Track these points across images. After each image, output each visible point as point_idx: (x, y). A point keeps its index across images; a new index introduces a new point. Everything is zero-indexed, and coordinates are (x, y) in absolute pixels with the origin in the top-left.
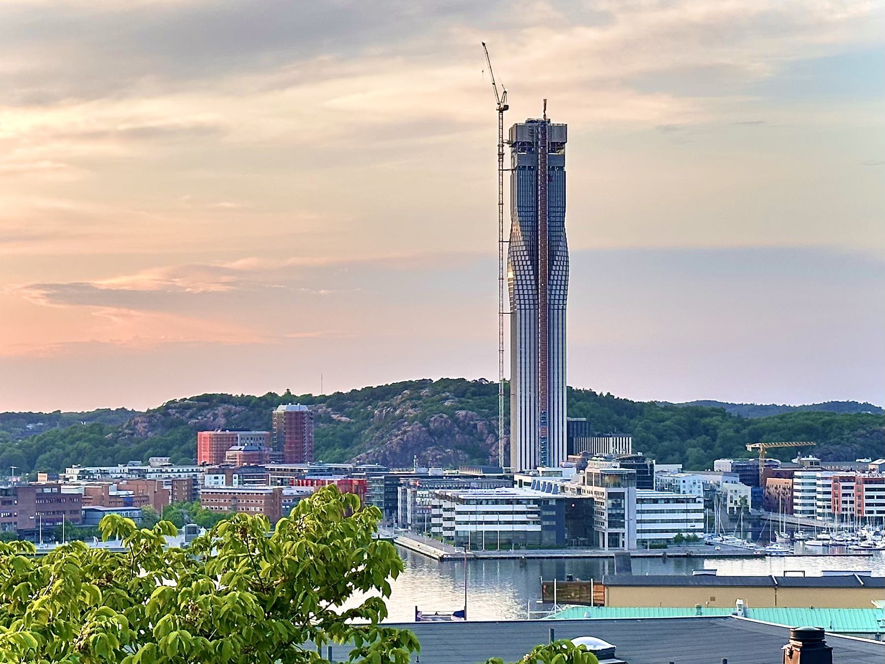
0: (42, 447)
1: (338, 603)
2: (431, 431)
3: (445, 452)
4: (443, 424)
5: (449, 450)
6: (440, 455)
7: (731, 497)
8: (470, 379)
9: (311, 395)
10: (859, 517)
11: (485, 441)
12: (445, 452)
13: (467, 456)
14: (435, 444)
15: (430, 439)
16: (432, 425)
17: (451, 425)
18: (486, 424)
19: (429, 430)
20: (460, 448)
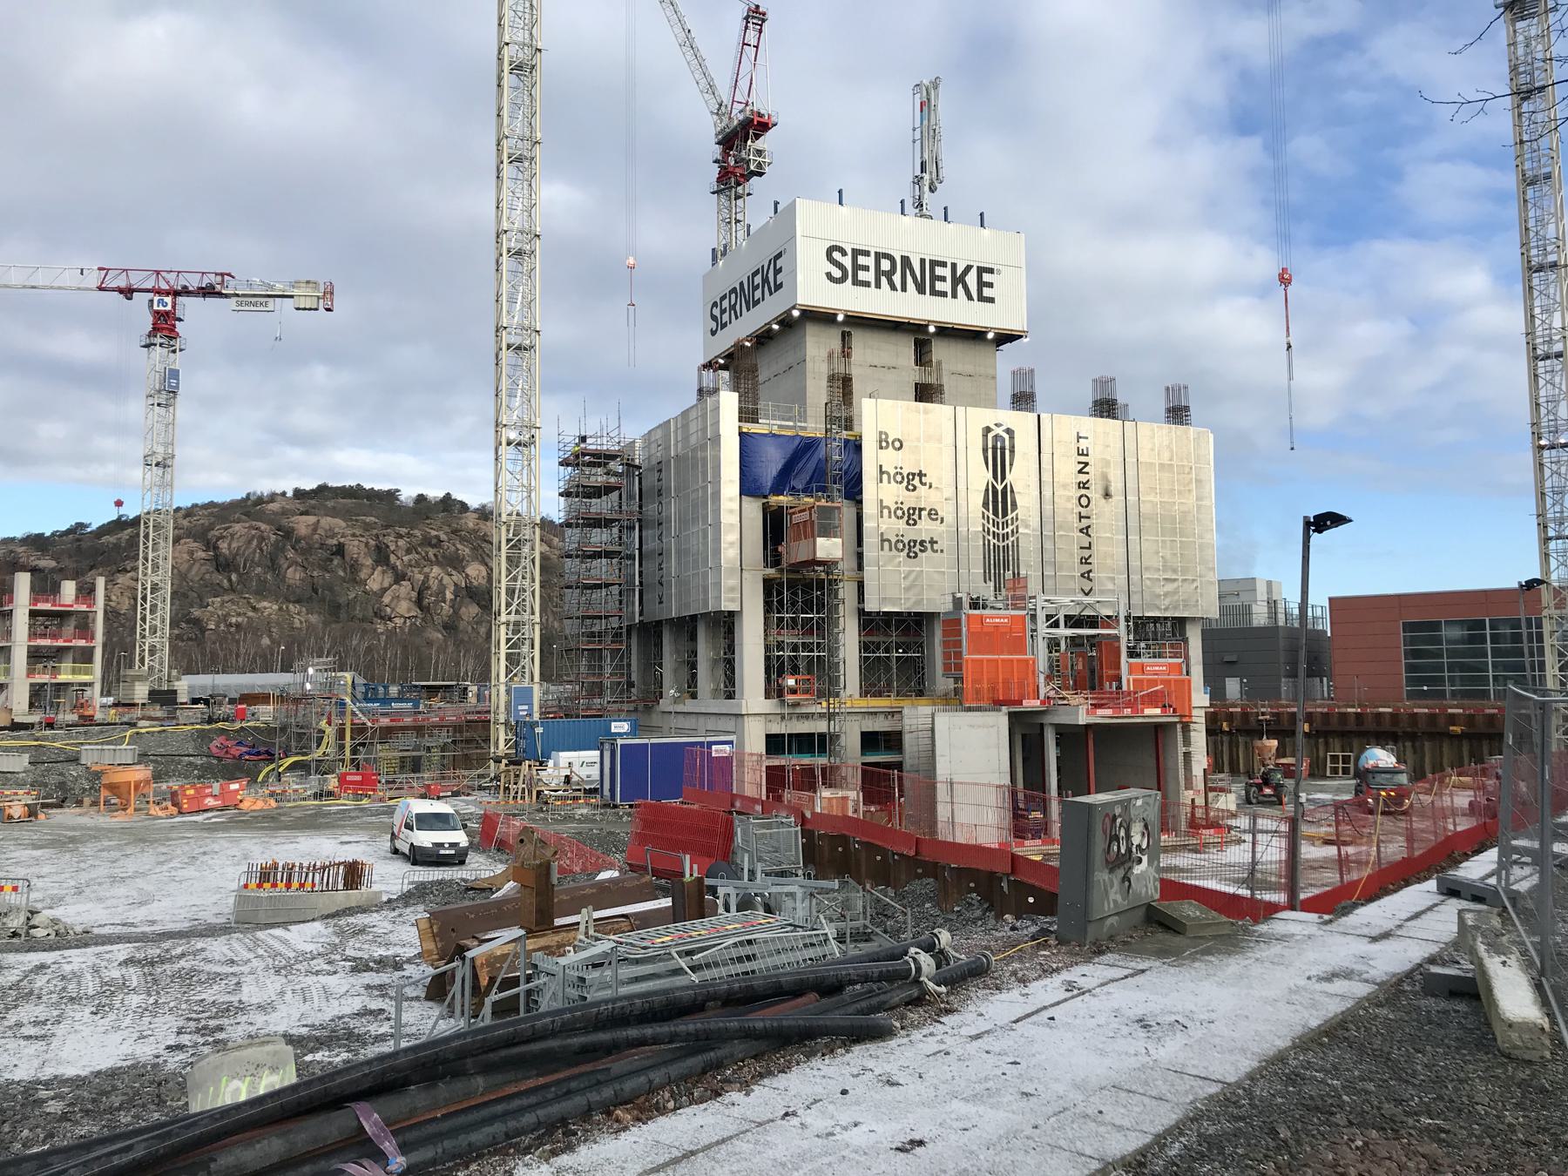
0: (783, 718)
1: (495, 1004)
2: (221, 559)
3: (254, 609)
4: (255, 542)
5: (265, 604)
6: (239, 615)
7: (988, 522)
8: (376, 489)
9: (80, 526)
10: (1439, 655)
11: (364, 583)
12: (254, 609)
13: (314, 618)
14: (232, 589)
15: (218, 578)
16: (226, 545)
17: (276, 545)
18: (367, 544)
19: (216, 557)
20: (298, 601)
